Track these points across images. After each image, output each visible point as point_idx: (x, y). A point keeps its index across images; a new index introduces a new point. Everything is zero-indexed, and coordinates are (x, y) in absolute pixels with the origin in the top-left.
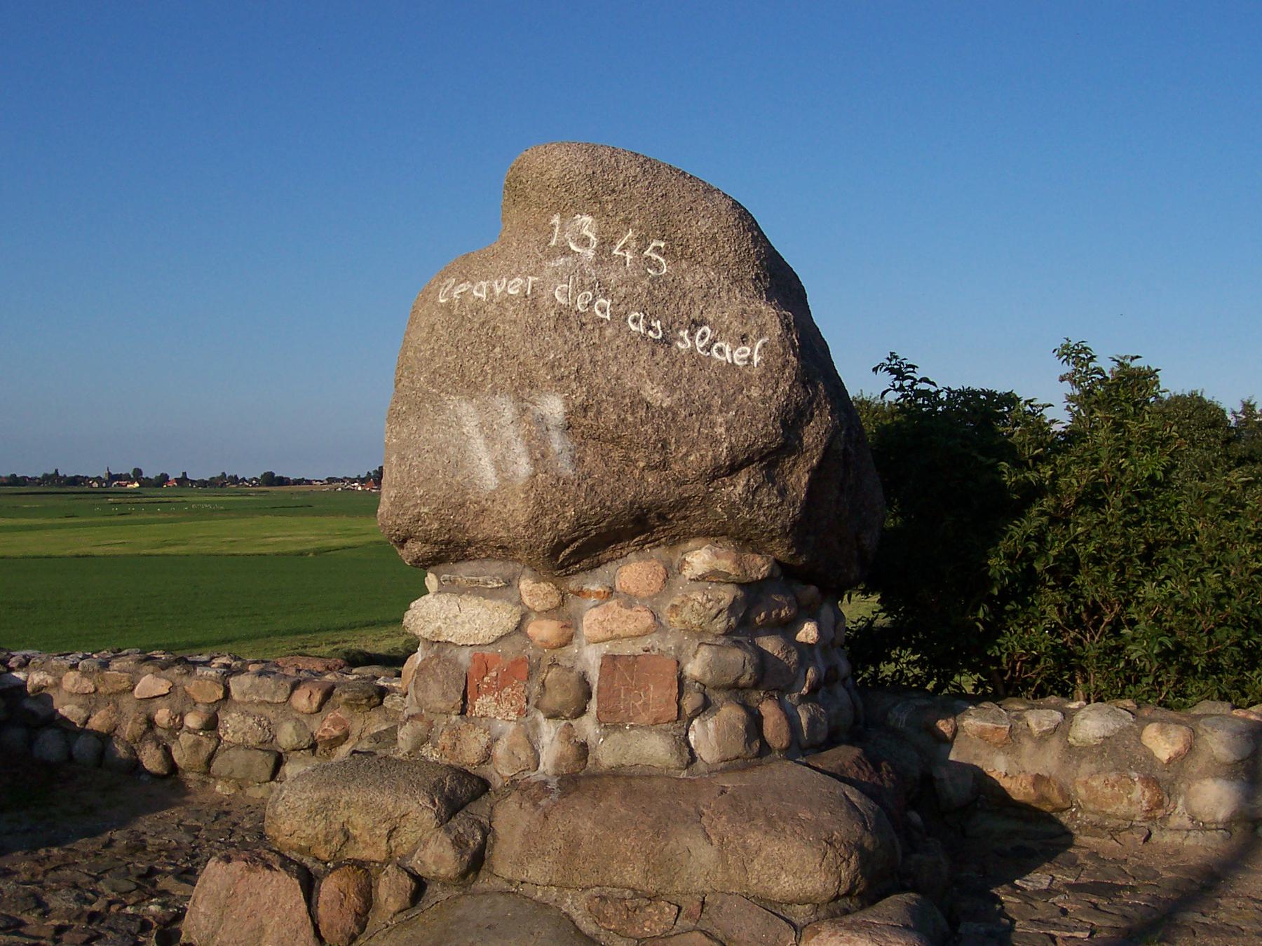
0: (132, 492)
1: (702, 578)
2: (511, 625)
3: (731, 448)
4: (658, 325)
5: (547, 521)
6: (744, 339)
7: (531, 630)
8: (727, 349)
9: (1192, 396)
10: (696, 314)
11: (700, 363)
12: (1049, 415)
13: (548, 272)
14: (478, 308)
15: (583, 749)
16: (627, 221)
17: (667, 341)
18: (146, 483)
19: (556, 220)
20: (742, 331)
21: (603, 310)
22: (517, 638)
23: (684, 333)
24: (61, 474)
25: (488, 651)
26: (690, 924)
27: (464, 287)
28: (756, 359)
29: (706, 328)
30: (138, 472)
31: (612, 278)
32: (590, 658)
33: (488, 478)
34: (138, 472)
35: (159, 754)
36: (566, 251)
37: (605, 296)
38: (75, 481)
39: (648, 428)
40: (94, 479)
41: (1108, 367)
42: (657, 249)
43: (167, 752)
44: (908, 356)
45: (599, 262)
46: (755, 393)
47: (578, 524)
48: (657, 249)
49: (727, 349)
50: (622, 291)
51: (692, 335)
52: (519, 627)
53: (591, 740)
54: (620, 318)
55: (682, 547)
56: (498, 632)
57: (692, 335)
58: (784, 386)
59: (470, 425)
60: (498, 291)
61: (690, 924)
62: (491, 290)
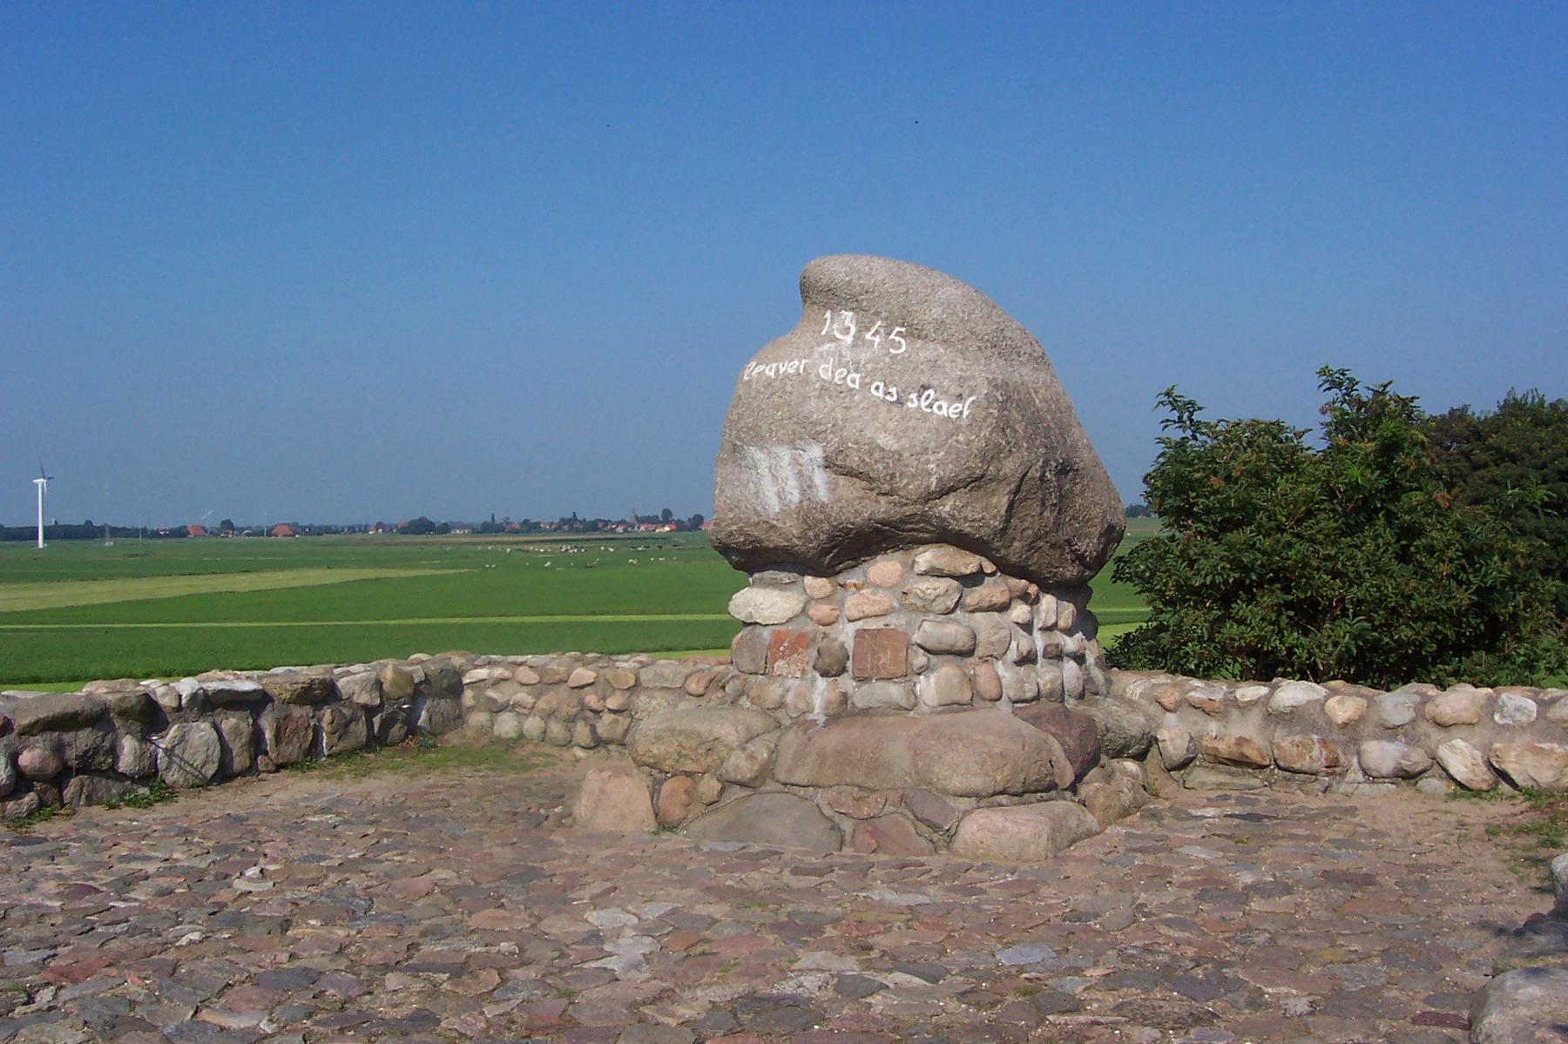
0: (664, 538)
1: (925, 573)
2: (799, 608)
3: (940, 480)
4: (893, 390)
5: (811, 533)
6: (960, 397)
7: (811, 612)
8: (945, 405)
9: (1500, 408)
10: (924, 381)
11: (925, 417)
12: (1306, 441)
13: (816, 355)
14: (769, 383)
15: (845, 697)
16: (877, 314)
17: (900, 402)
18: (680, 526)
19: (828, 314)
20: (960, 390)
21: (853, 381)
22: (802, 619)
23: (913, 396)
24: (580, 518)
25: (782, 628)
26: (892, 809)
27: (762, 367)
28: (966, 413)
29: (931, 392)
30: (667, 514)
31: (863, 357)
32: (846, 634)
33: (774, 506)
34: (667, 514)
35: (587, 730)
36: (834, 339)
37: (857, 370)
38: (594, 526)
39: (880, 466)
40: (618, 523)
41: (1366, 395)
42: (899, 334)
43: (593, 729)
44: (1186, 392)
45: (854, 345)
46: (961, 438)
47: (831, 538)
48: (899, 334)
49: (945, 405)
50: (869, 366)
51: (920, 396)
52: (804, 611)
53: (850, 691)
54: (865, 386)
55: (914, 552)
56: (790, 614)
57: (920, 396)
58: (986, 432)
59: (763, 469)
60: (782, 370)
61: (892, 809)
62: (778, 369)
